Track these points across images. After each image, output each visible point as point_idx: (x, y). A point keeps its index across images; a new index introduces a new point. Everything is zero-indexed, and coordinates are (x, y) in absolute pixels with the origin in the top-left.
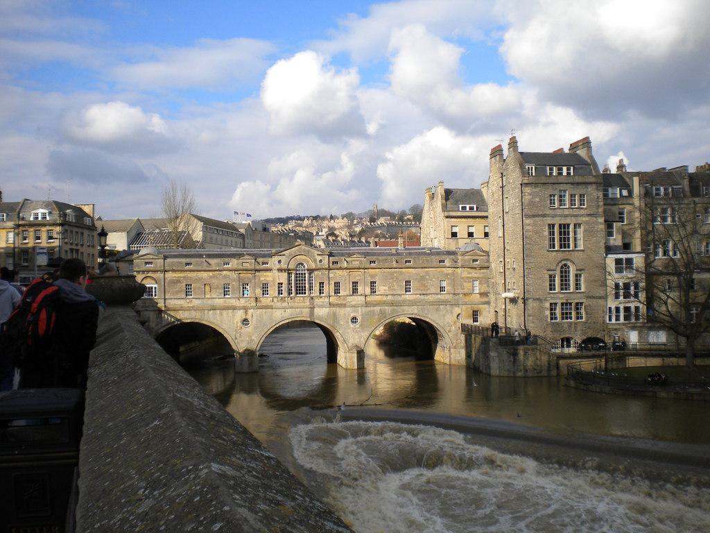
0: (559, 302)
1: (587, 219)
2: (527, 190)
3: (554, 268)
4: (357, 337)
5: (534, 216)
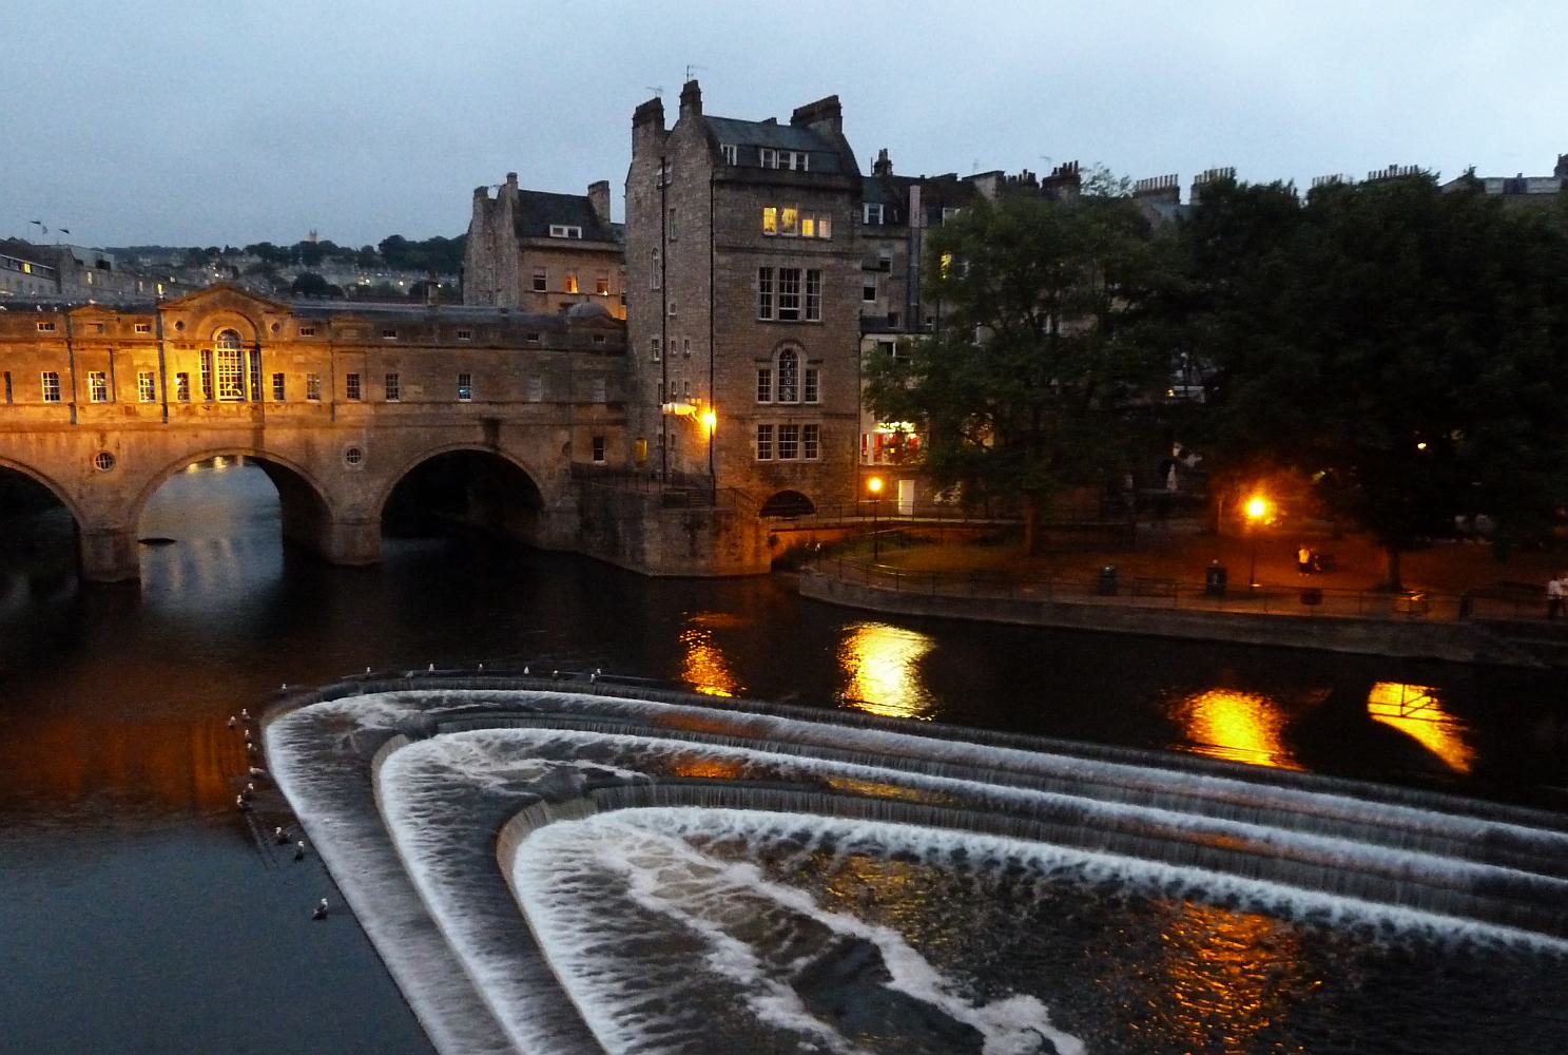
0: (776, 422)
1: (831, 261)
2: (726, 194)
3: (767, 356)
4: (359, 491)
5: (732, 250)
